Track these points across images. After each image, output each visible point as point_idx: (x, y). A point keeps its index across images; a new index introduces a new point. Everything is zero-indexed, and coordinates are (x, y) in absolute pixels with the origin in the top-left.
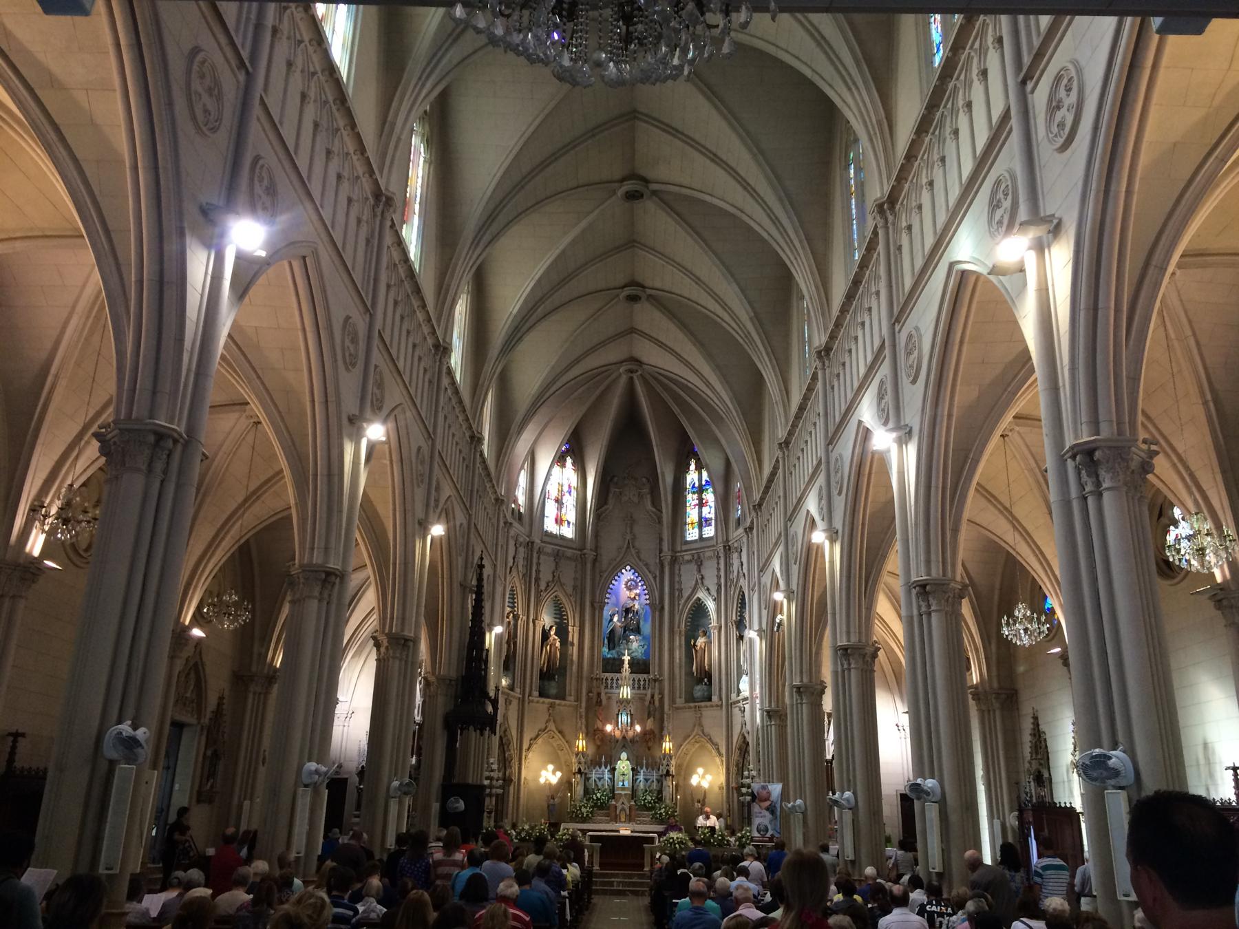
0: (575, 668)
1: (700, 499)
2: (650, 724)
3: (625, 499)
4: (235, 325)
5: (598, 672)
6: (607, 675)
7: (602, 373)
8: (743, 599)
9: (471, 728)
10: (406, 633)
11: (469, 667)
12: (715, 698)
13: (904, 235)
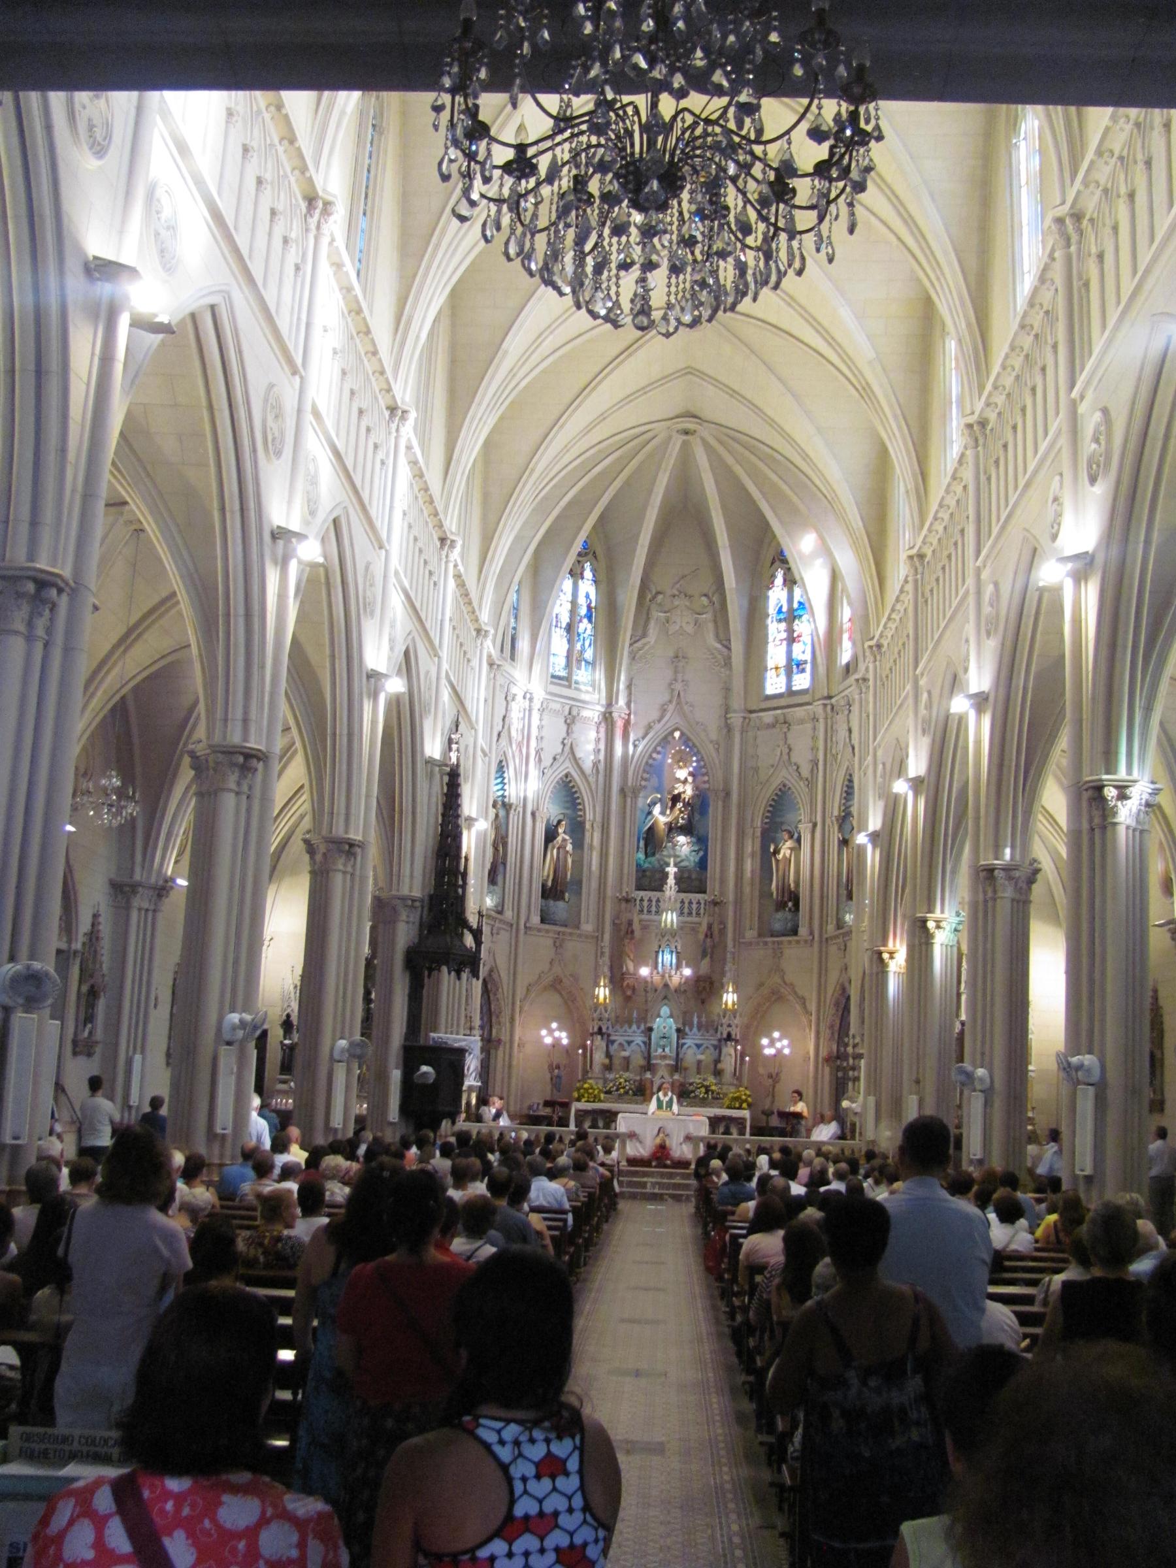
0: (594, 884)
1: (790, 631)
2: (705, 965)
3: (673, 628)
4: (129, 417)
5: (629, 888)
6: (642, 893)
9: (445, 969)
10: (351, 836)
11: (439, 883)
12: (803, 931)
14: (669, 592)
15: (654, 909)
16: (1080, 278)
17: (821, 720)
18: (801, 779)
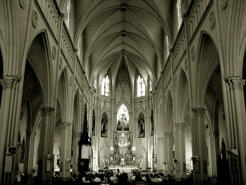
3: (122, 86)
5: (116, 130)
6: (118, 131)
14: (121, 80)
15: (120, 134)
16: (189, 25)
18: (144, 111)
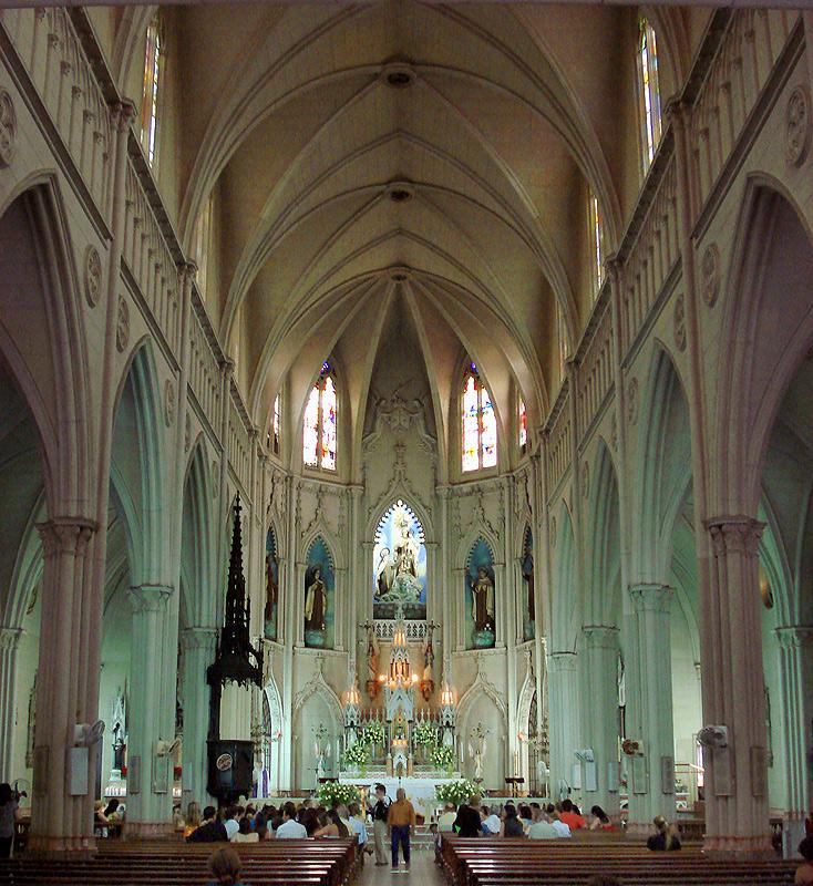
6: (379, 621)
7: (365, 284)
8: (529, 532)
13: (700, 139)
15: (388, 632)
17: (506, 489)
